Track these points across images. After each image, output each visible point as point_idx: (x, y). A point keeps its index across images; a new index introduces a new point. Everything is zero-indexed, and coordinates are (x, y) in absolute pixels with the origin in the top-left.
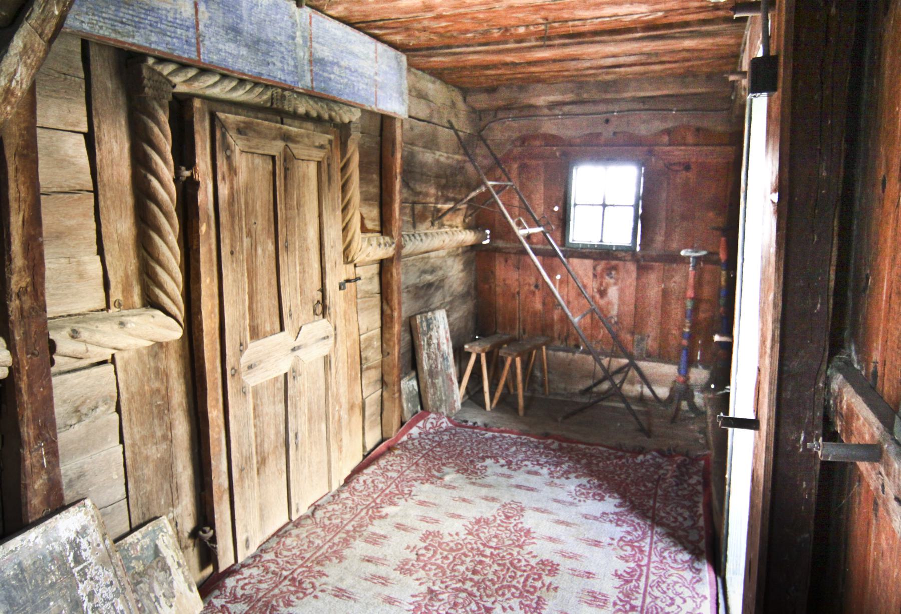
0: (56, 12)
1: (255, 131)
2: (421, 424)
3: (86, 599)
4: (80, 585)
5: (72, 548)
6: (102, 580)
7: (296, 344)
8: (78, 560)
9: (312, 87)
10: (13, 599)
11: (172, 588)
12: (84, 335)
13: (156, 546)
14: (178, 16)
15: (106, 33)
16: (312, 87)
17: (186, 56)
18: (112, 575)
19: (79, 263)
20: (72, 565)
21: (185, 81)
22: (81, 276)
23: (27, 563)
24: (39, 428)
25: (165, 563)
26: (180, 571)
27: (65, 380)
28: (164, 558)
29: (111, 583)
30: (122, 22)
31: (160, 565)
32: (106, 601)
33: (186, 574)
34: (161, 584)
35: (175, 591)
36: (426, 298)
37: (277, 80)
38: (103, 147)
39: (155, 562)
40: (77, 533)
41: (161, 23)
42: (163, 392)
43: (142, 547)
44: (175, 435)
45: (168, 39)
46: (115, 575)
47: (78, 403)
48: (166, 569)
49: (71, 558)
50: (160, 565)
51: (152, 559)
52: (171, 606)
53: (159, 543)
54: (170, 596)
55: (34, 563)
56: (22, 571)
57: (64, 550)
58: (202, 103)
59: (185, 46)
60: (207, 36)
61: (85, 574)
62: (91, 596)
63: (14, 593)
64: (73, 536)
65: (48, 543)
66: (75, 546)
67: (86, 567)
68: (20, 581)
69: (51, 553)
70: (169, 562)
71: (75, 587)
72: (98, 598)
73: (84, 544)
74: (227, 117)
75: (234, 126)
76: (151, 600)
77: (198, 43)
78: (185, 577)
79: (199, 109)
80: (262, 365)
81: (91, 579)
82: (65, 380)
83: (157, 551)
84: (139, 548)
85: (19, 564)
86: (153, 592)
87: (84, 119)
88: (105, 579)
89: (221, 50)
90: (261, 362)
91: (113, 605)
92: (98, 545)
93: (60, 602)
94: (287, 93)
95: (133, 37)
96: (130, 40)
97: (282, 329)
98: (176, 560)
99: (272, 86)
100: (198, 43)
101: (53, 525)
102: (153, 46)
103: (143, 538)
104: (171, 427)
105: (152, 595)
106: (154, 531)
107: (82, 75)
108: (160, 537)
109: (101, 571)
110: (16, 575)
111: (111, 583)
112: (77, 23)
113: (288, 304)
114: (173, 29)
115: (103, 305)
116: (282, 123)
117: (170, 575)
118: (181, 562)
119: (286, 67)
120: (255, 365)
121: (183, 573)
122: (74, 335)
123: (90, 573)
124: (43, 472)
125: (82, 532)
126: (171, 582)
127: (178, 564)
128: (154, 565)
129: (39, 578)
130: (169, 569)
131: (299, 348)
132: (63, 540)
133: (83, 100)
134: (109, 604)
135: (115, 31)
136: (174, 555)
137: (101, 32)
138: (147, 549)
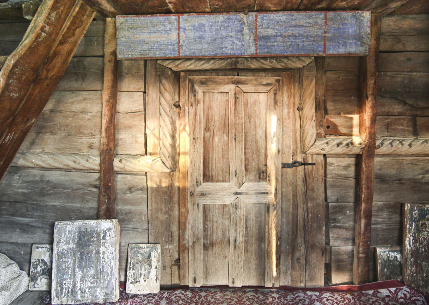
0: (13, 62)
1: (213, 82)
2: (393, 289)
3: (102, 253)
4: (102, 247)
5: (103, 233)
6: (109, 250)
7: (239, 191)
8: (104, 238)
9: (257, 53)
10: (81, 238)
11: (149, 274)
12: (124, 161)
13: (150, 254)
14: (169, 41)
15: (138, 56)
16: (257, 53)
17: (173, 56)
18: (114, 251)
19: (136, 137)
20: (102, 239)
21: (175, 66)
22: (137, 142)
23: (89, 230)
24: (106, 189)
25: (151, 263)
26: (156, 270)
27: (127, 177)
28: (151, 261)
29: (112, 253)
30: (144, 51)
31: (148, 262)
32: (108, 258)
33: (158, 273)
34: (145, 270)
35: (149, 276)
36: (177, 169)
37: (228, 55)
38: (149, 96)
39: (147, 260)
40: (107, 229)
41: (161, 46)
42: (169, 193)
43: (144, 251)
44: (173, 214)
45: (164, 51)
46: (115, 251)
47: (131, 186)
48: (150, 265)
49: (102, 236)
50: (148, 262)
51: (146, 257)
52: (145, 281)
53: (152, 254)
54: (147, 277)
55: (91, 231)
56: (86, 231)
57: (101, 232)
58: (171, 73)
59: (172, 52)
60: (184, 45)
61: (105, 245)
62: (104, 253)
63: (82, 237)
64: (105, 229)
65: (97, 227)
66: (105, 233)
67: (105, 242)
68: (85, 234)
69: (97, 231)
70: (153, 263)
71: (99, 246)
72: (106, 255)
73: (108, 234)
74: (194, 78)
75: (199, 81)
76: (139, 273)
77: (179, 49)
78: (156, 274)
79: (183, 76)
80: (211, 196)
81: (106, 247)
82: (127, 177)
83: (149, 256)
84: (143, 251)
85: (87, 229)
86: (141, 270)
87: (143, 86)
88: (111, 251)
89: (192, 49)
90: (210, 194)
91: (110, 261)
92: (113, 237)
93: (94, 248)
94: (239, 60)
95: (148, 55)
96: (147, 56)
97: (230, 182)
98: (156, 265)
99: (230, 58)
100: (179, 49)
101: (100, 222)
102: (157, 56)
103: (147, 248)
104: (171, 209)
105: (140, 272)
106: (152, 248)
107: (144, 72)
108: (154, 251)
109: (110, 246)
110: (84, 232)
111: (112, 253)
112: (127, 56)
113: (235, 168)
114: (166, 47)
115: (144, 153)
116: (238, 75)
117: (151, 269)
118: (158, 267)
119: (235, 47)
120: (206, 194)
121: (156, 272)
122: (120, 161)
123: (106, 245)
124: (105, 204)
125: (109, 230)
126: (150, 272)
127: (156, 267)
128: (146, 261)
129: (90, 236)
130: (151, 266)
131: (240, 193)
132: (102, 229)
133: (143, 81)
134: (109, 260)
135: (141, 54)
136: (156, 262)
137: (136, 56)
138: (146, 253)
